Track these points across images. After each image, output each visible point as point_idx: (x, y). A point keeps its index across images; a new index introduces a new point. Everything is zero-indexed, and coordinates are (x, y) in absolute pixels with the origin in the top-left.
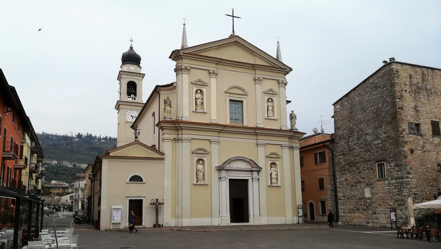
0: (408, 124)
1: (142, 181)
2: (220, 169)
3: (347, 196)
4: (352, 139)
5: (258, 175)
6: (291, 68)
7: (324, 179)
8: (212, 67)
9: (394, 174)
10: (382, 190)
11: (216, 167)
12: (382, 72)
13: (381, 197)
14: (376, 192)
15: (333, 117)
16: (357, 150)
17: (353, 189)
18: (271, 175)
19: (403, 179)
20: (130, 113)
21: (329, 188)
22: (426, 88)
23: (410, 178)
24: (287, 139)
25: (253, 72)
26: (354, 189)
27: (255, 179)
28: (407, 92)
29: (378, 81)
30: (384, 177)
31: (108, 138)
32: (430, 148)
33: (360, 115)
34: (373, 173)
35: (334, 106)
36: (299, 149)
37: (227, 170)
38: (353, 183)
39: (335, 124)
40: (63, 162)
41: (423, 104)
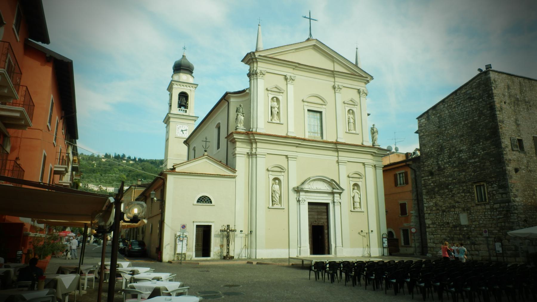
0: (511, 140)
1: (211, 202)
2: (298, 190)
3: (437, 223)
4: (442, 157)
5: (340, 198)
6: (373, 77)
7: (407, 203)
8: (289, 72)
9: (497, 197)
10: (483, 216)
11: (294, 188)
12: (477, 81)
13: (481, 224)
14: (475, 219)
15: (416, 132)
16: (449, 170)
17: (446, 216)
18: (353, 198)
19: (510, 203)
20: (180, 127)
21: (412, 214)
22: (525, 100)
23: (517, 202)
24: (370, 157)
25: (332, 80)
26: (447, 215)
27: (337, 202)
28: (506, 104)
29: (473, 91)
30: (484, 200)
31: (137, 160)
32: (535, 168)
33: (451, 130)
34: (470, 197)
35: (418, 120)
36: (382, 168)
37: (307, 192)
38: (444, 208)
39: (421, 140)
40: (89, 185)
41: (523, 117)
